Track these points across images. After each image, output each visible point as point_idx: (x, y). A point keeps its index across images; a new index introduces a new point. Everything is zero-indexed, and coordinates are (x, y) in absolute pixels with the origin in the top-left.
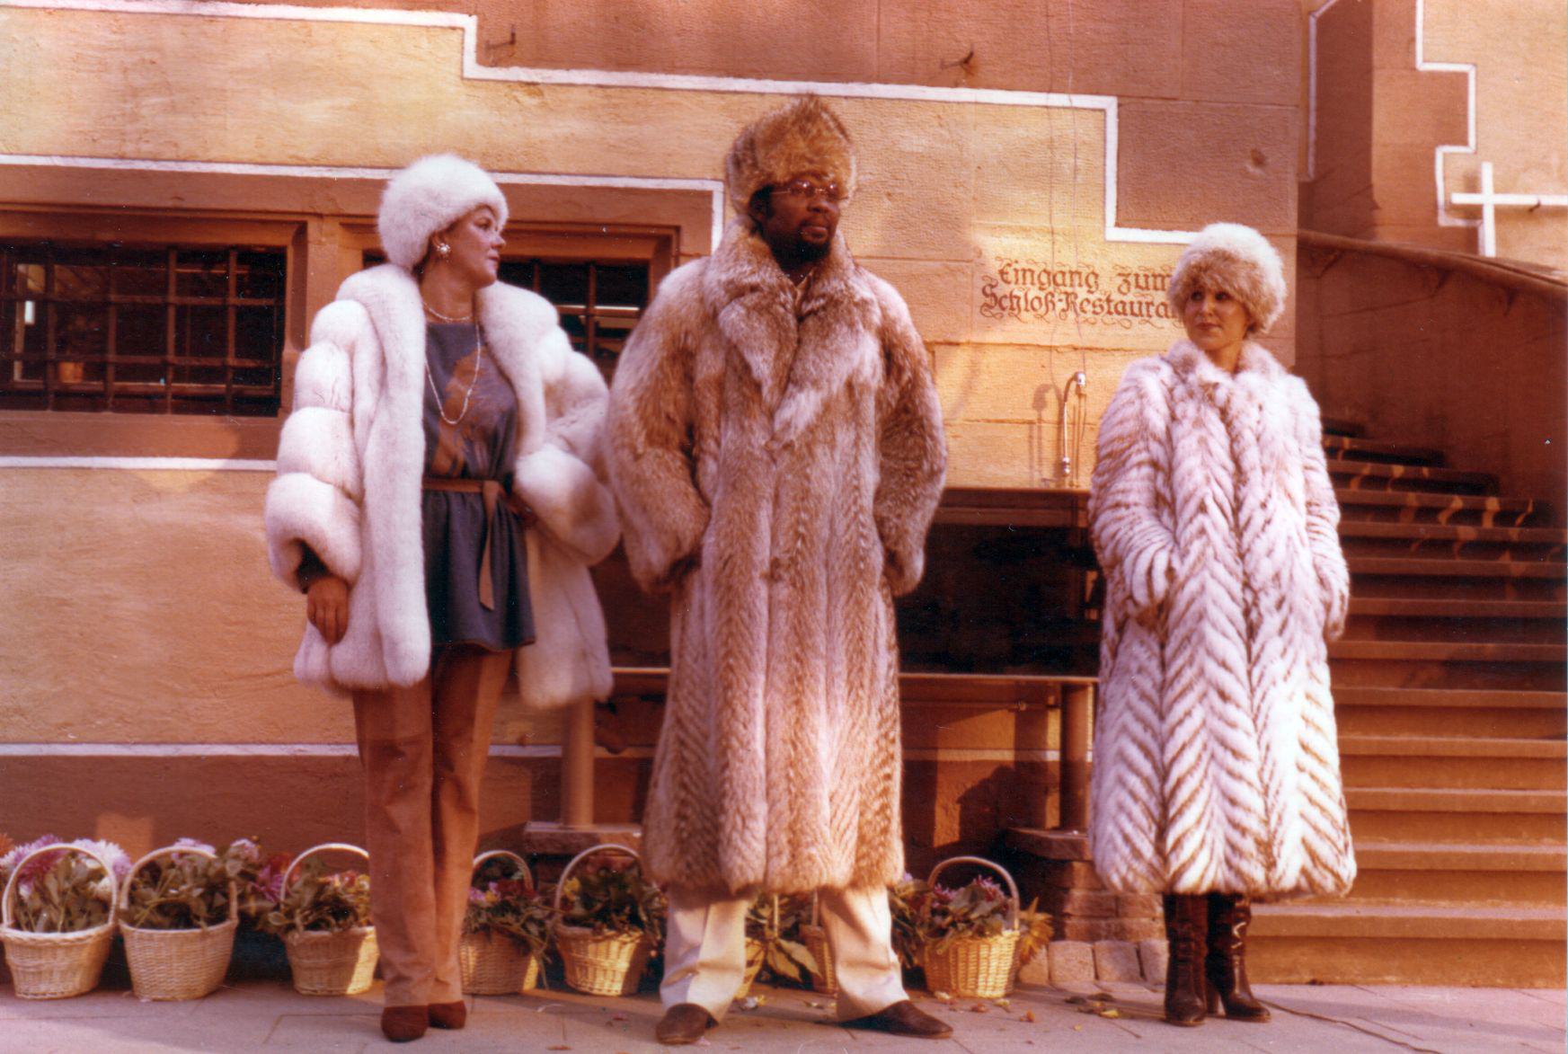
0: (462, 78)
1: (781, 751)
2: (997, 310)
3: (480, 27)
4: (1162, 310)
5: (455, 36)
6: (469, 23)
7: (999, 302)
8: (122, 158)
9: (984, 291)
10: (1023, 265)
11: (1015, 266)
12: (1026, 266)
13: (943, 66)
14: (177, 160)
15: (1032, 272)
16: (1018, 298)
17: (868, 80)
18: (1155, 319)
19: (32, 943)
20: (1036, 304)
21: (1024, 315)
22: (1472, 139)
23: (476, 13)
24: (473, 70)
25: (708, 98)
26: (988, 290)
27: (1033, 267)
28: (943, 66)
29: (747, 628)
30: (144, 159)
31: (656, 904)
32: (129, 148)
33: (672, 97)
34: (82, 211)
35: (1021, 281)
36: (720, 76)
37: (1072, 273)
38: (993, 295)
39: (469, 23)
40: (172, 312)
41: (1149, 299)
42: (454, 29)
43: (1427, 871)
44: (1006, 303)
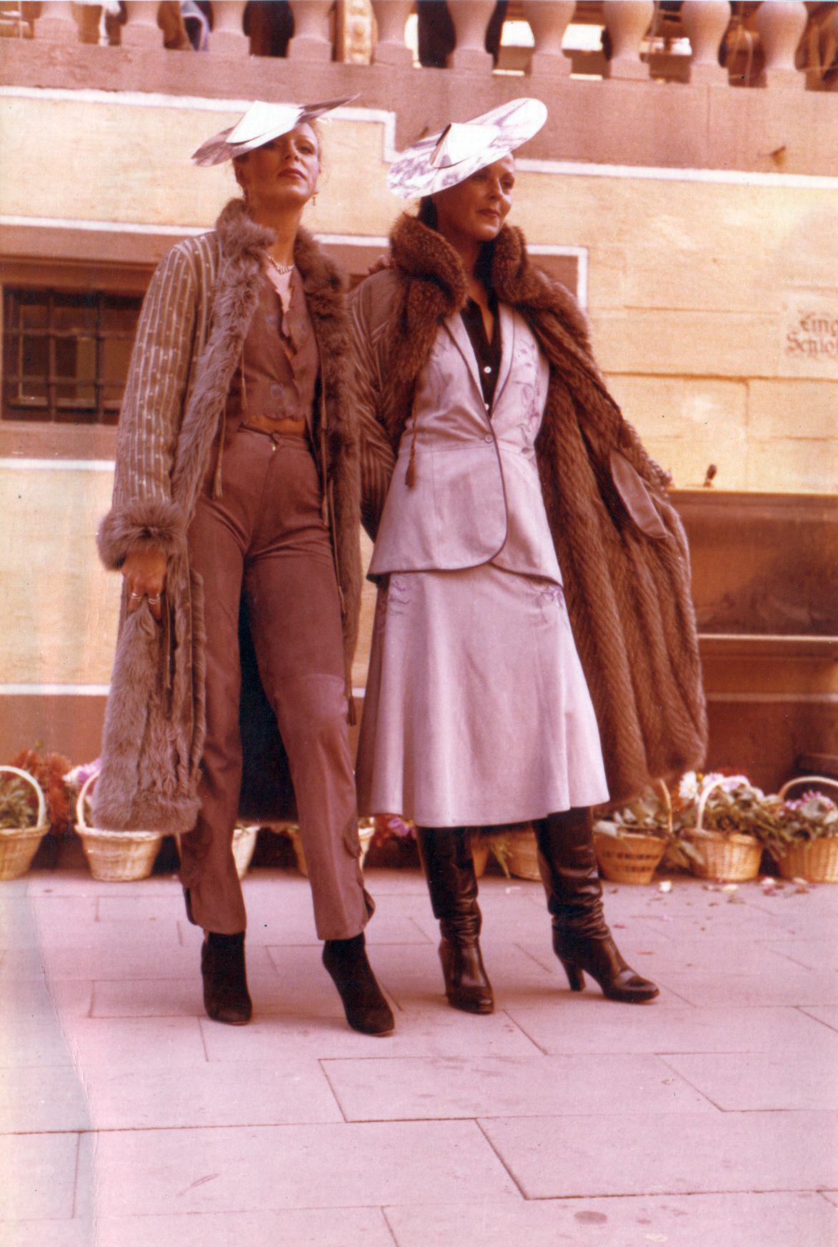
0: (384, 162)
1: (651, 711)
2: (798, 352)
3: (399, 121)
5: (378, 129)
6: (388, 118)
7: (799, 346)
8: (115, 221)
9: (789, 338)
10: (817, 317)
11: (813, 318)
12: (823, 318)
13: (759, 155)
14: (184, 225)
15: (826, 322)
16: (815, 342)
17: (699, 166)
19: (114, 840)
20: (829, 348)
21: (820, 355)
23: (394, 110)
24: (395, 157)
25: (576, 181)
26: (792, 336)
27: (828, 319)
28: (759, 155)
29: (603, 611)
30: (132, 223)
31: (617, 816)
32: (121, 214)
33: (545, 179)
34: (62, 263)
35: (817, 329)
36: (583, 162)
37: (820, 322)
38: (796, 341)
39: (388, 118)
40: (52, 343)
42: (376, 123)
43: (594, 1197)
44: (806, 346)
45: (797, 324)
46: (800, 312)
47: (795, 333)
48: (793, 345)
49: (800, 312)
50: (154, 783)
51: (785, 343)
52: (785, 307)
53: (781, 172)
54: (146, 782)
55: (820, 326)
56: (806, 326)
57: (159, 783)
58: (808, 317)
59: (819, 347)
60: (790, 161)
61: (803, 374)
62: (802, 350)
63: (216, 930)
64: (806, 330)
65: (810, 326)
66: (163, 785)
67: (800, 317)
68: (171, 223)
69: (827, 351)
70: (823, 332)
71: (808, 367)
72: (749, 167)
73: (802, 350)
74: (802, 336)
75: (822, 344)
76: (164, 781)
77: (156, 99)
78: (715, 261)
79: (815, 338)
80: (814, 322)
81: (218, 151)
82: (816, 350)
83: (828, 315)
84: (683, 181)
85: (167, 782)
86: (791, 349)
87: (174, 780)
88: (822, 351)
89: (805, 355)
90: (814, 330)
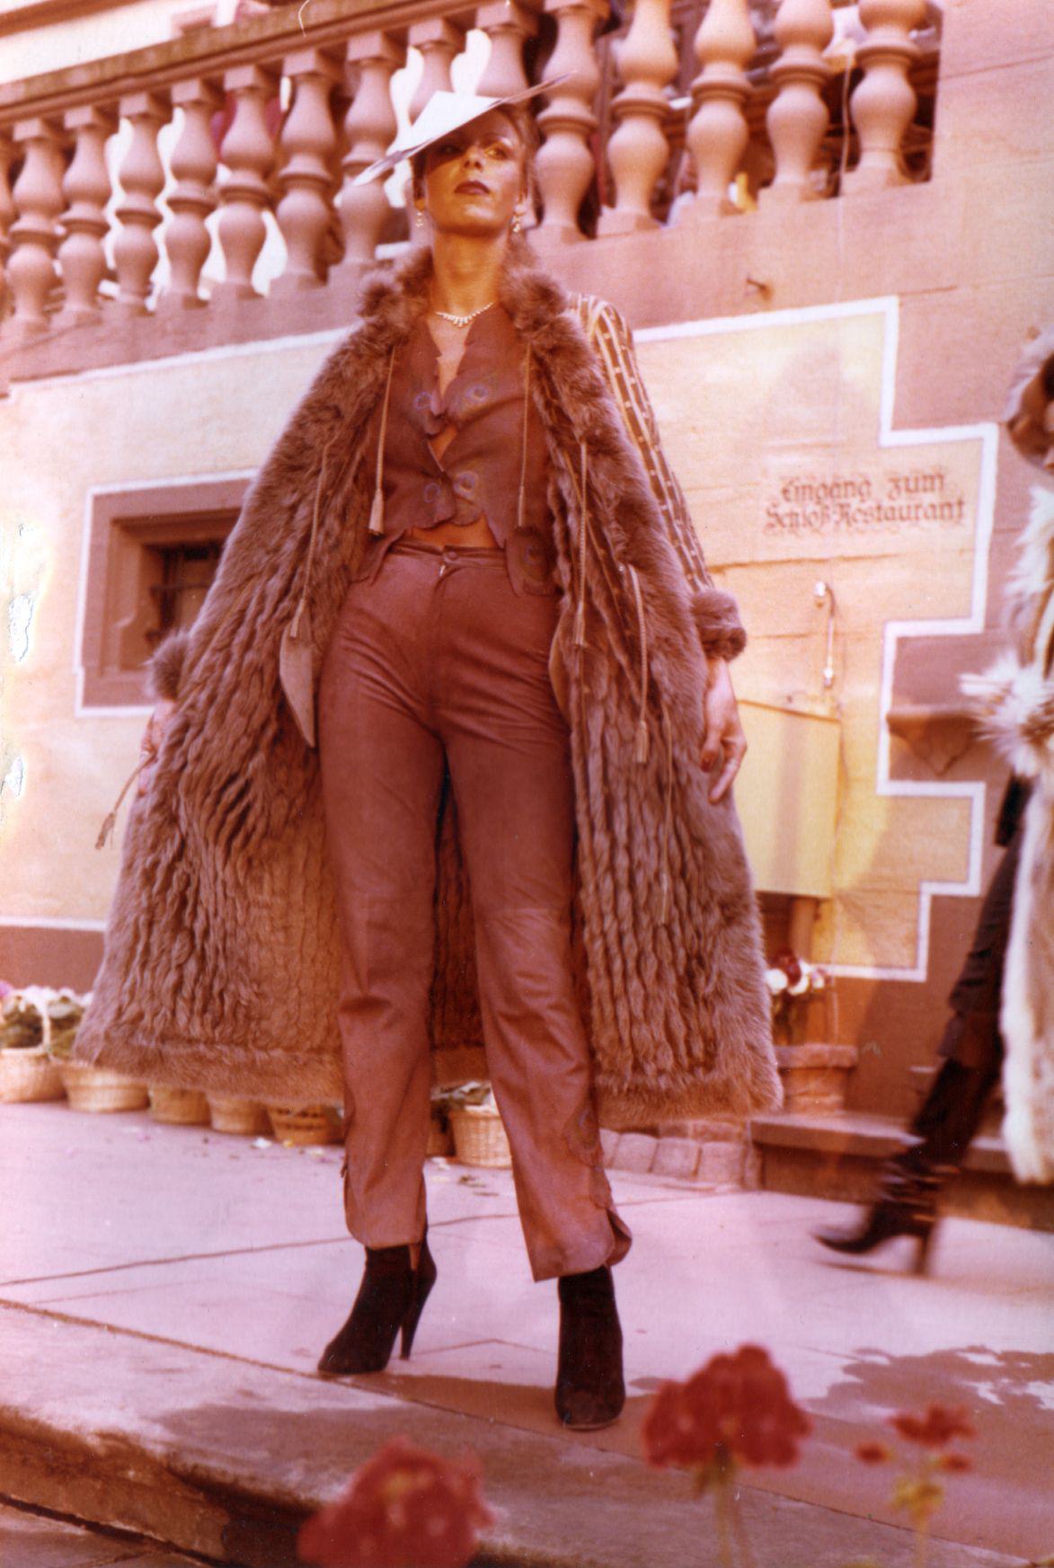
2: (778, 528)
4: (930, 512)
9: (769, 514)
11: (797, 484)
16: (797, 515)
18: (923, 523)
20: (813, 519)
22: (925, 903)
37: (804, 487)
38: (776, 515)
41: (917, 502)
44: (787, 521)
45: (777, 493)
46: (782, 478)
47: (775, 506)
48: (773, 520)
49: (782, 478)
50: (141, 1016)
51: (764, 519)
52: (765, 472)
53: (767, 309)
54: (130, 1012)
55: (804, 494)
56: (787, 495)
57: (147, 1018)
58: (791, 483)
59: (801, 520)
60: (778, 294)
61: (782, 556)
62: (783, 526)
63: (370, 1244)
64: (788, 500)
65: (792, 495)
66: (152, 1020)
67: (781, 485)
68: (231, 468)
69: (810, 523)
70: (807, 501)
71: (806, 544)
72: (735, 309)
73: (783, 526)
74: (784, 508)
75: (804, 516)
76: (156, 1014)
77: (228, 351)
78: (694, 429)
79: (798, 510)
80: (797, 488)
81: (394, 347)
82: (797, 524)
83: (813, 478)
84: (665, 341)
85: (160, 1016)
86: (771, 526)
87: (169, 1014)
88: (804, 525)
89: (785, 530)
90: (797, 500)
